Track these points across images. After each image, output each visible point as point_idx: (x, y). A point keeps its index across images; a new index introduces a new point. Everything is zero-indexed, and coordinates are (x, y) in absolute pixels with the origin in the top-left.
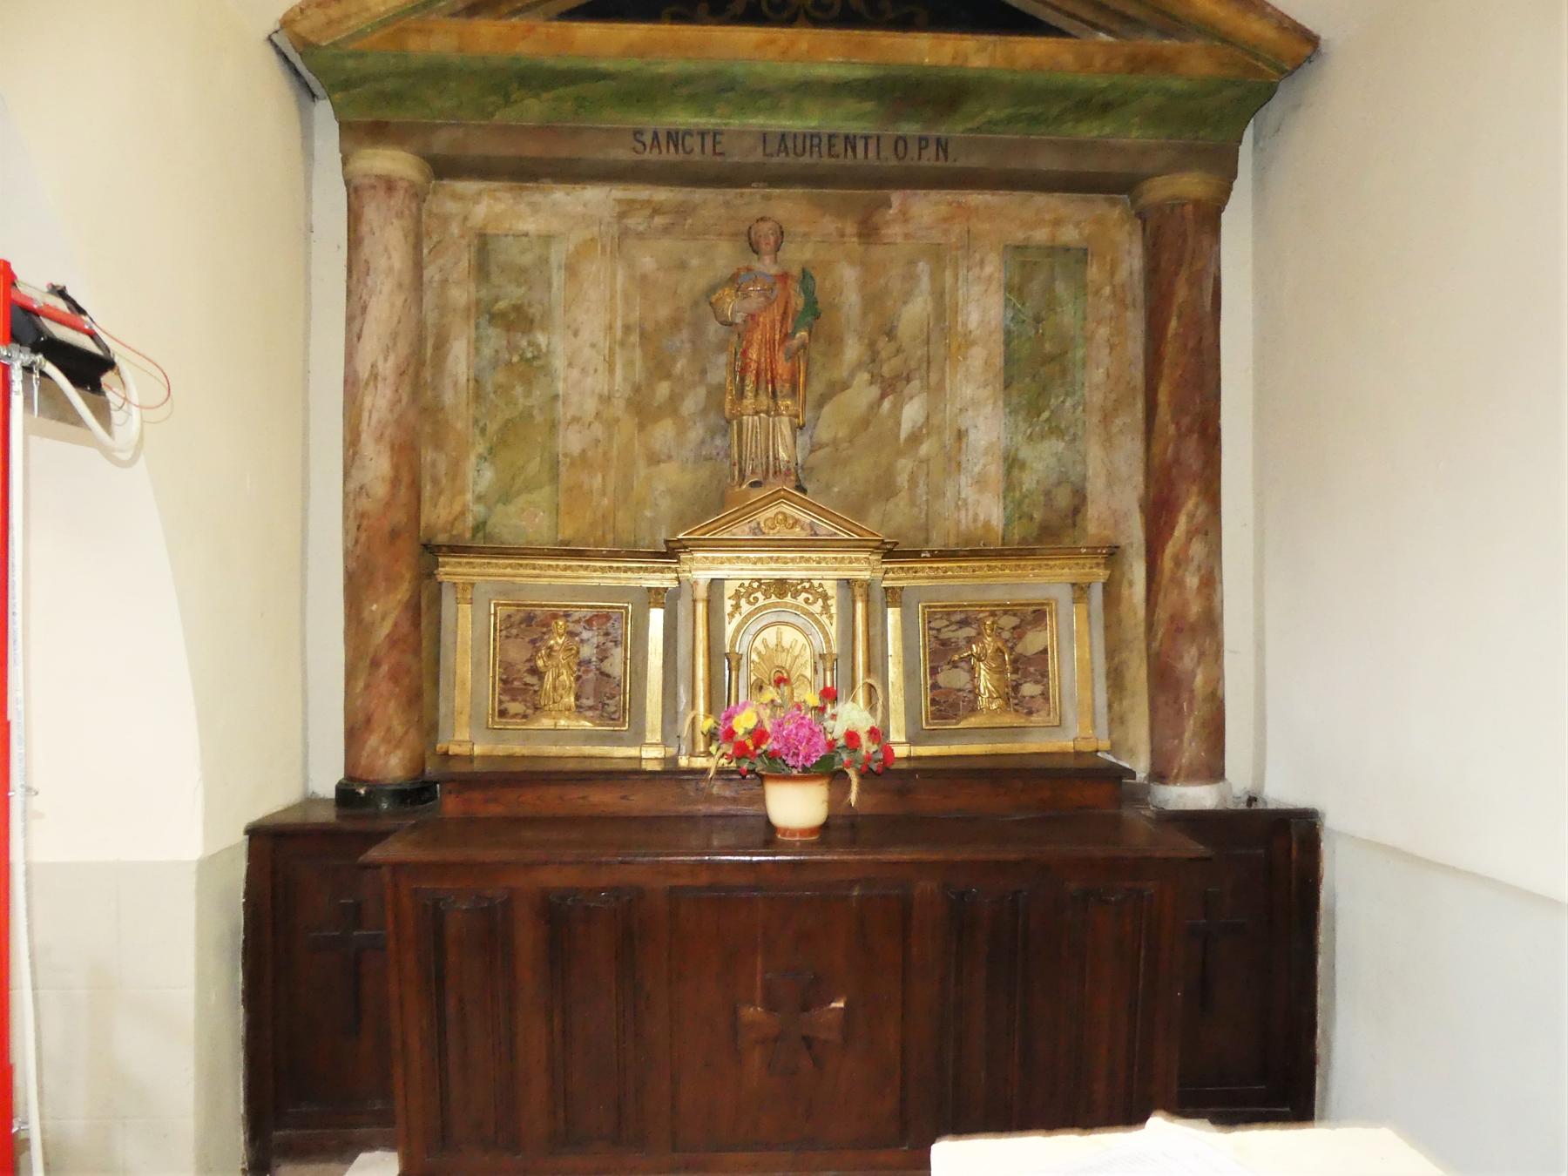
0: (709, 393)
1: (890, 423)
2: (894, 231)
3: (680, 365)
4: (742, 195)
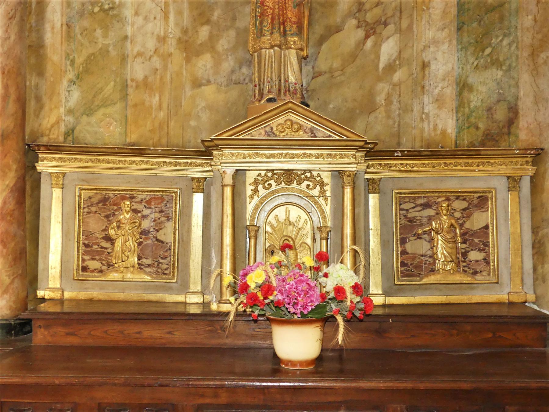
0: (238, 34)
1: (373, 57)
3: (216, 14)
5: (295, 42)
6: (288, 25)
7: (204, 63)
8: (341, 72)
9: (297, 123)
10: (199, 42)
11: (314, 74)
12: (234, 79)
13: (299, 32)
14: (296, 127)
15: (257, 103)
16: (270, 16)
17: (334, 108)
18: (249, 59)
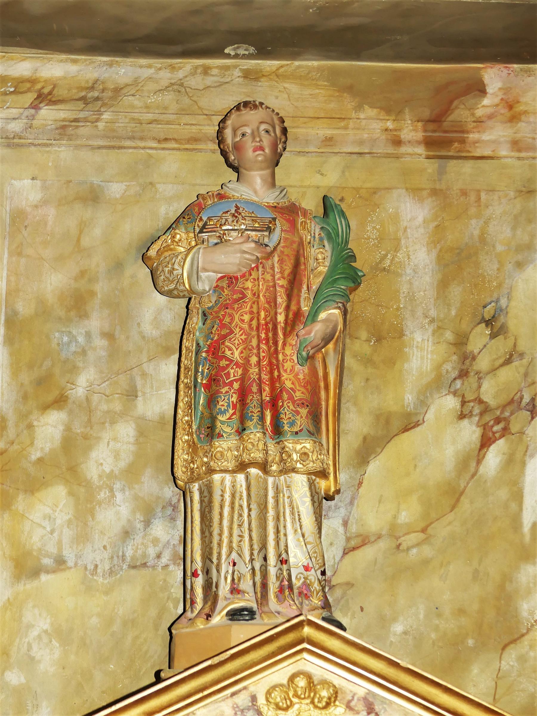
0: (141, 433)
1: (503, 494)
2: (493, 137)
3: (82, 384)
4: (206, 71)
5: (304, 455)
6: (287, 410)
7: (48, 511)
8: (421, 536)
9: (325, 683)
10: (35, 455)
11: (348, 539)
12: (129, 553)
13: (314, 432)
14: (325, 694)
15: (200, 624)
16: (236, 386)
17: (405, 633)
18: (193, 502)
